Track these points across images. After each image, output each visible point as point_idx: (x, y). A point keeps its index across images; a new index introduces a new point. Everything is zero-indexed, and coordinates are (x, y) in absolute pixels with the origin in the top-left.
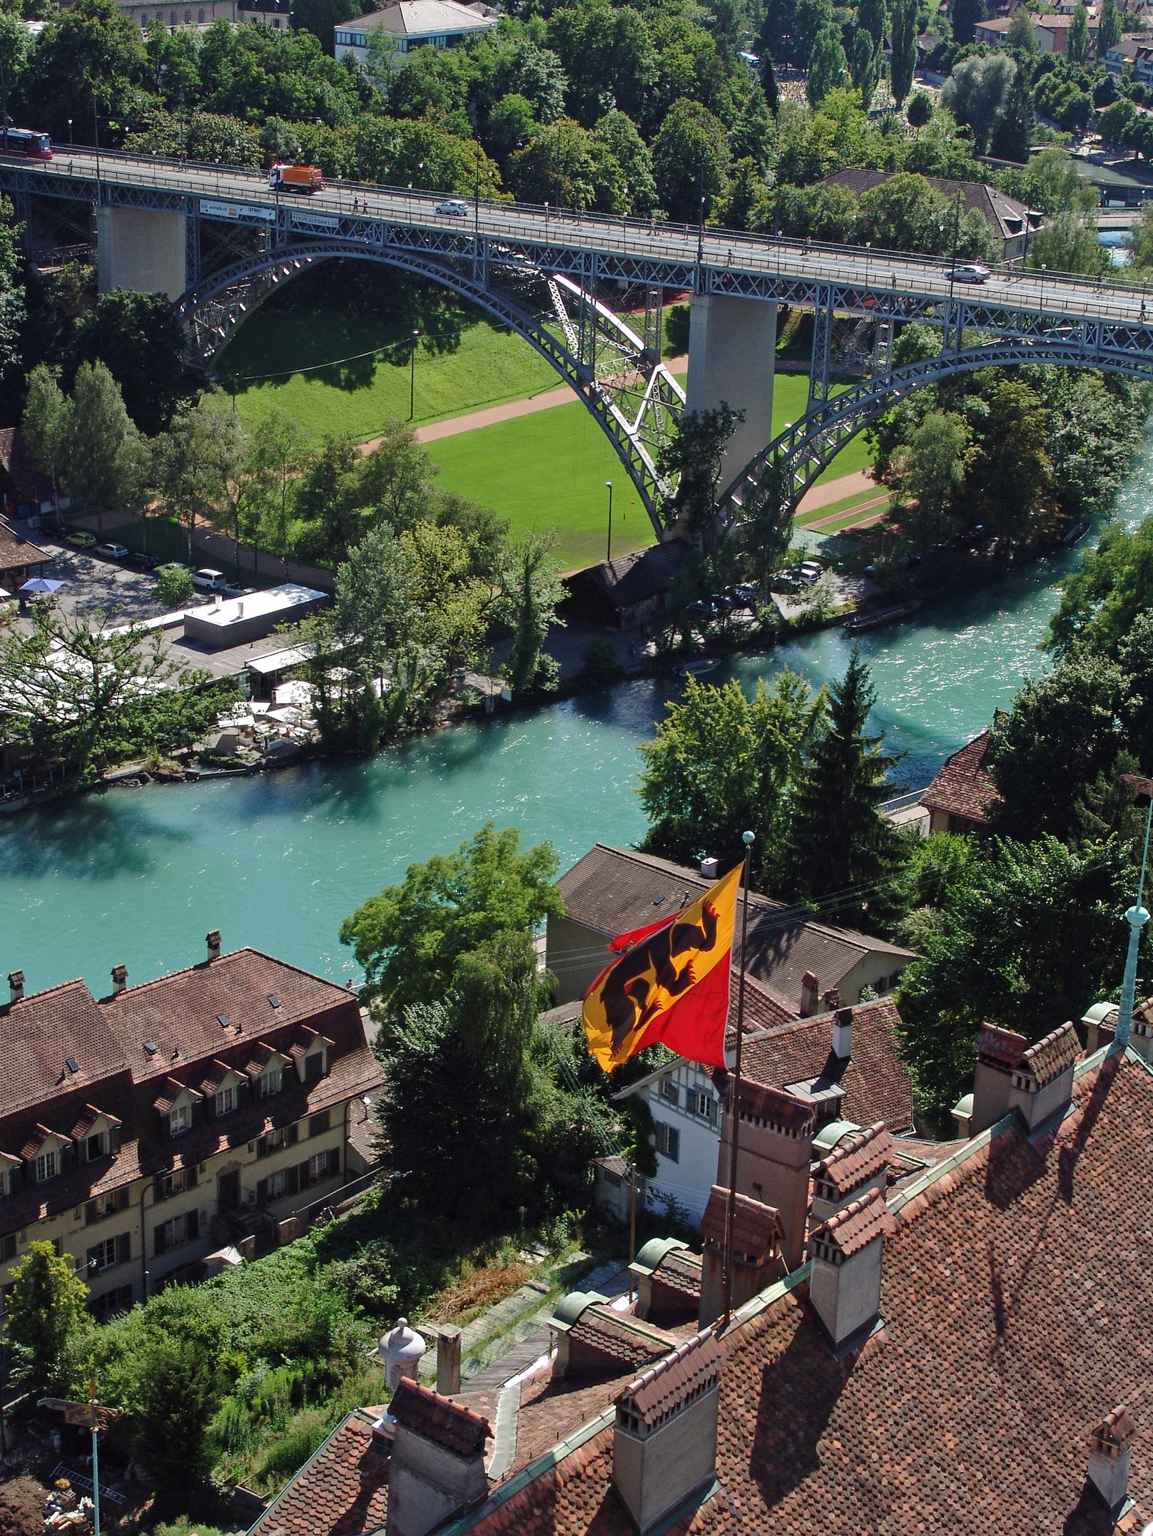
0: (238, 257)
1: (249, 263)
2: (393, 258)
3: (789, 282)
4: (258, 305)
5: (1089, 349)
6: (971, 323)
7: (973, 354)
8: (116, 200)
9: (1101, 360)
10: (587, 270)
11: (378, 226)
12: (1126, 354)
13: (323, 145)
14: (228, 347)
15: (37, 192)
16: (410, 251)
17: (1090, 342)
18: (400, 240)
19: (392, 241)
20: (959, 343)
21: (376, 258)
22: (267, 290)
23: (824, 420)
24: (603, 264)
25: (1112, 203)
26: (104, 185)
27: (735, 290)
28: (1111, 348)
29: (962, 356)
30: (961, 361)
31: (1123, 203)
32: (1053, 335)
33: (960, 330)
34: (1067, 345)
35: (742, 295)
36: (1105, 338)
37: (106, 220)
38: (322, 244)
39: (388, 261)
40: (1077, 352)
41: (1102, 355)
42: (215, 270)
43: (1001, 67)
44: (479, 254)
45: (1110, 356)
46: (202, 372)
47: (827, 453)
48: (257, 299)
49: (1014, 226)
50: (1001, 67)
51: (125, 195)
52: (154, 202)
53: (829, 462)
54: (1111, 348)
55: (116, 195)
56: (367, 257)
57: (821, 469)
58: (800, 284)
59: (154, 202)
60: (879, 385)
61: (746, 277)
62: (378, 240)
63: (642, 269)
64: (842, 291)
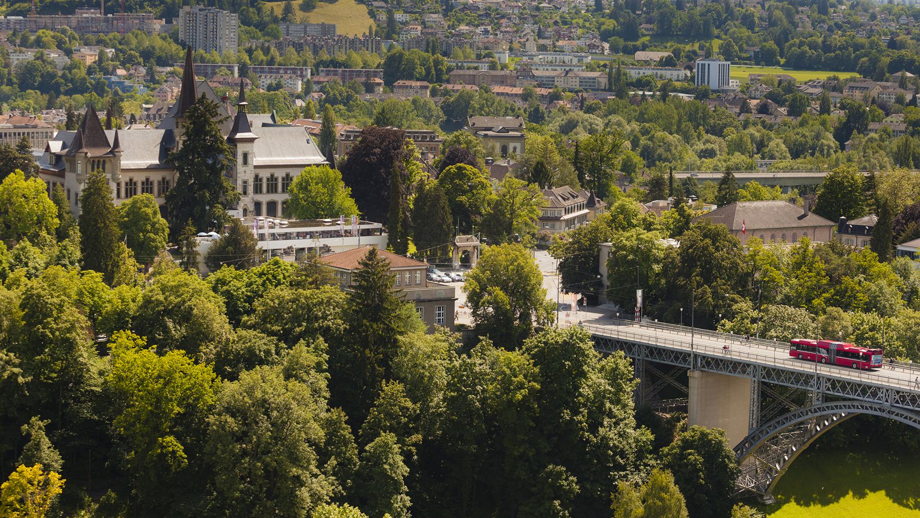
0: (788, 410)
1: (794, 415)
2: (897, 415)
4: (804, 448)
8: (704, 367)
11: (819, 378)
13: (871, 330)
14: (782, 478)
15: (767, 381)
16: (911, 411)
18: (903, 402)
19: (897, 402)
21: (884, 415)
22: (812, 436)
24: (764, 373)
26: (696, 356)
27: (908, 404)
35: (715, 371)
37: (695, 378)
38: (847, 403)
39: (893, 417)
41: (893, 409)
42: (771, 419)
43: (471, 97)
46: (762, 496)
48: (804, 443)
50: (471, 97)
51: (711, 363)
52: (730, 368)
55: (704, 362)
56: (878, 413)
59: (730, 368)
62: (887, 401)
63: (851, 389)
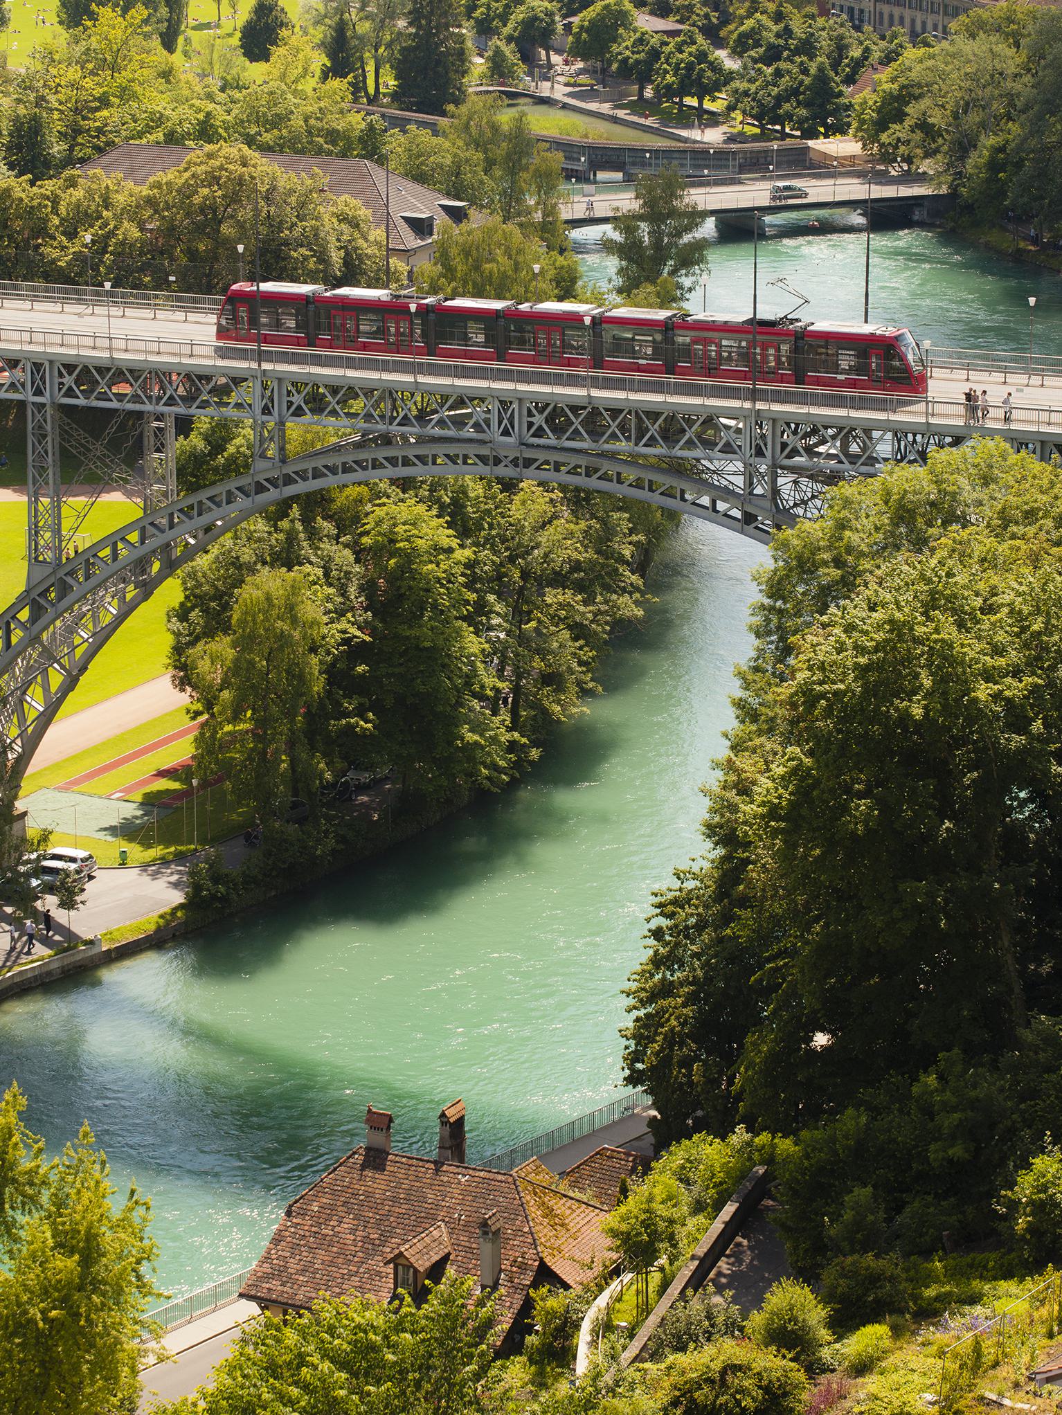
3: (200, 377)
5: (506, 446)
6: (299, 412)
7: (309, 465)
9: (528, 463)
10: (38, 392)
12: (459, 440)
17: (506, 433)
19: (539, 433)
20: (282, 449)
23: (60, 598)
25: (601, 176)
28: (541, 441)
29: (289, 469)
30: (288, 480)
31: (619, 176)
32: (441, 423)
33: (281, 424)
34: (471, 441)
36: (530, 425)
40: (484, 451)
41: (529, 454)
44: (38, 392)
45: (541, 456)
47: (79, 652)
49: (421, 227)
53: (83, 669)
54: (541, 441)
57: (71, 683)
58: (350, 388)
60: (151, 530)
61: (595, 412)
64: (70, 368)
